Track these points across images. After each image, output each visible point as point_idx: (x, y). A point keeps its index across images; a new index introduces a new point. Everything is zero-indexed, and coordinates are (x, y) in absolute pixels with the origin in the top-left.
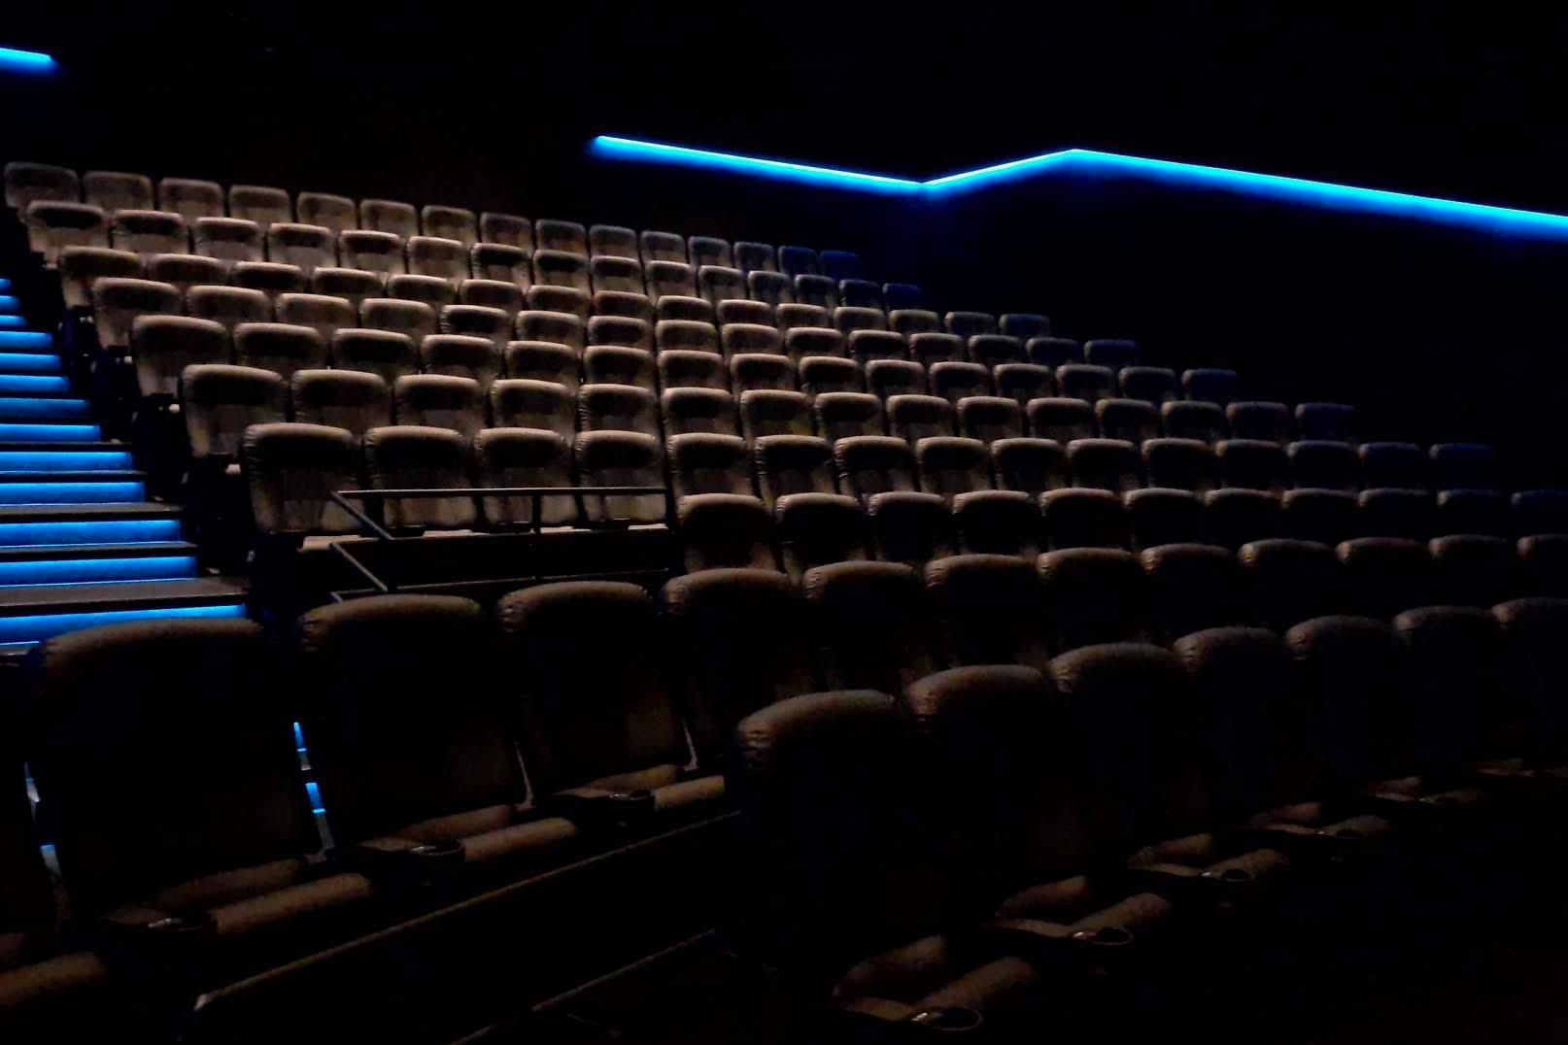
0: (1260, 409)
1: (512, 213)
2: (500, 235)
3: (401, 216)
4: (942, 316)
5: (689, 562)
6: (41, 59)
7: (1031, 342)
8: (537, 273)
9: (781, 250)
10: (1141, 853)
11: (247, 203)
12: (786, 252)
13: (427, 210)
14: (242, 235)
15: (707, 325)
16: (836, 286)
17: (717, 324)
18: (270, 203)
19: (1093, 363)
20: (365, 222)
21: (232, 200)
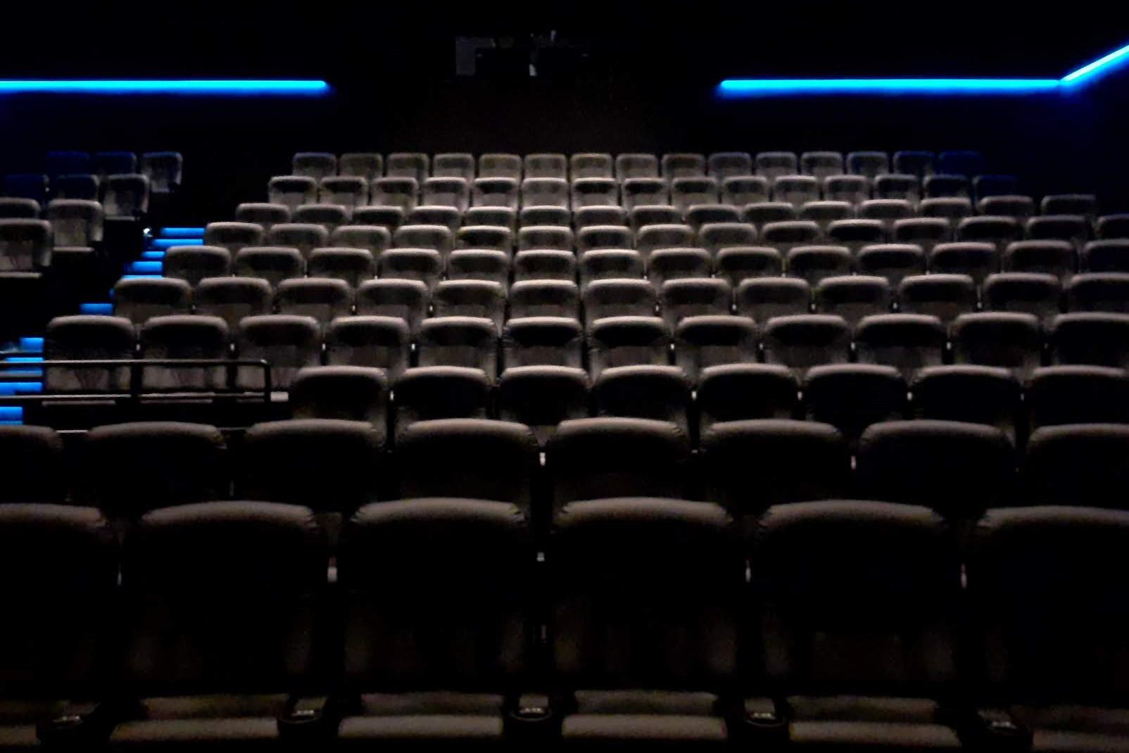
0: (1100, 282)
1: (686, 151)
2: (631, 171)
3: (646, 164)
4: (1037, 201)
5: (570, 359)
6: (318, 85)
7: (1102, 219)
8: (624, 198)
9: (897, 156)
10: (331, 515)
11: (811, 166)
12: (901, 158)
13: (666, 157)
14: (805, 187)
15: (566, 229)
16: (920, 183)
17: (573, 226)
18: (829, 163)
19: (1104, 237)
20: (850, 170)
21: (802, 163)
